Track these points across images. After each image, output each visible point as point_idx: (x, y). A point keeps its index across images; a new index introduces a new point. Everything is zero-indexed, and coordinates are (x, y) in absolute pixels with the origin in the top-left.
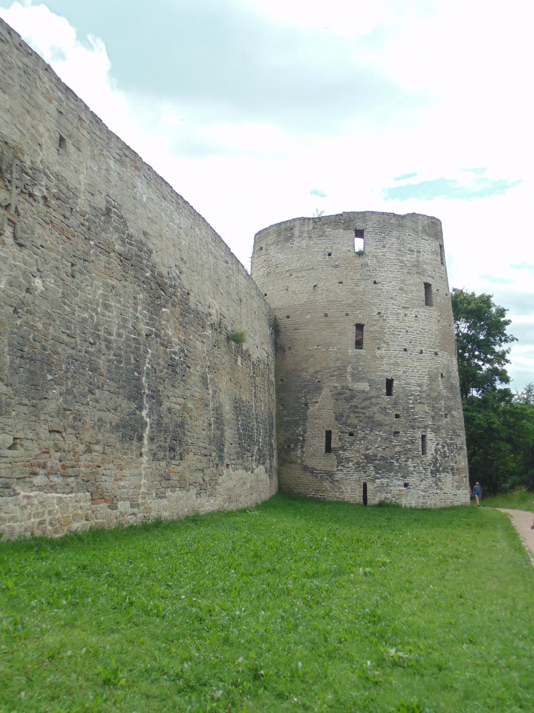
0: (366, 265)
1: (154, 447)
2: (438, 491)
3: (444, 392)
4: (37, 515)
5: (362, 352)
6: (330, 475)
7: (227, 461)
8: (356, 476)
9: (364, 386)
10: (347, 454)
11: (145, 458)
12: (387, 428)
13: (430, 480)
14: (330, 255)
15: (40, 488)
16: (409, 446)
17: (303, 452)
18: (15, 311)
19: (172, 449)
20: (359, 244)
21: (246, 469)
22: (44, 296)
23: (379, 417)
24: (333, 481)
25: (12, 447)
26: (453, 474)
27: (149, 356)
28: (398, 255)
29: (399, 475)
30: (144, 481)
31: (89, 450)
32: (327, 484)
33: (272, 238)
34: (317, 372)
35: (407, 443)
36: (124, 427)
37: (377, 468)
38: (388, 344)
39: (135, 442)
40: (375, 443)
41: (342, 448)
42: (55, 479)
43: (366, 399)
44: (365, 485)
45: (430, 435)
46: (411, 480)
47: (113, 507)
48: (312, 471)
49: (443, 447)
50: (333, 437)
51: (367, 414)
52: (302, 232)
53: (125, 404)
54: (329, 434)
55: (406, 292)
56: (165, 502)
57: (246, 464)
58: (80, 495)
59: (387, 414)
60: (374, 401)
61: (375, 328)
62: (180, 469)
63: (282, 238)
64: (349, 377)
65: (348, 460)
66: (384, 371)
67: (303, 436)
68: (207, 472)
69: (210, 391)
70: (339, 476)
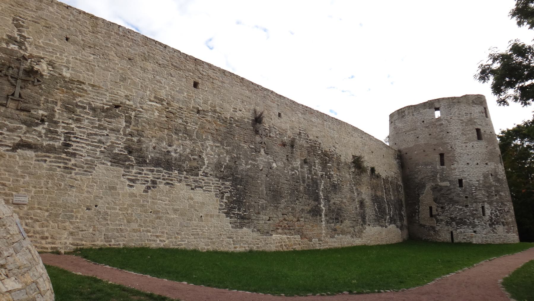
0: (442, 124)
1: (328, 218)
2: (495, 234)
3: (494, 183)
4: (279, 243)
5: (445, 167)
6: (433, 228)
7: (368, 223)
8: (446, 228)
9: (447, 184)
10: (441, 218)
11: (324, 223)
12: (461, 203)
13: (489, 229)
14: (423, 122)
15: (280, 234)
16: (475, 212)
17: (419, 218)
18: (267, 176)
19: (336, 219)
20: (437, 114)
21: (382, 226)
22: (277, 169)
23: (456, 198)
24: (435, 231)
25: (269, 220)
26: (504, 225)
27: (323, 183)
28: (459, 117)
29: (470, 227)
30: (324, 231)
31: (298, 220)
32: (432, 233)
33: (396, 117)
34: (422, 179)
35: (473, 210)
36: (313, 211)
37: (457, 224)
38: (457, 162)
39: (318, 217)
40: (456, 211)
41: (438, 215)
42: (286, 231)
43: (449, 190)
44: (452, 233)
45: (486, 206)
46: (478, 229)
47: (311, 241)
48: (424, 226)
49: (496, 211)
50: (433, 209)
51: (450, 197)
52: (409, 113)
53: (313, 202)
54: (431, 208)
55: (465, 135)
56: (335, 240)
57: (381, 224)
58: (296, 236)
59: (460, 197)
60: (453, 190)
61: (450, 155)
62: (341, 226)
63: (400, 116)
64: (438, 180)
65: (442, 220)
66: (456, 175)
67: (418, 210)
68: (356, 228)
69: (356, 194)
70: (437, 228)
